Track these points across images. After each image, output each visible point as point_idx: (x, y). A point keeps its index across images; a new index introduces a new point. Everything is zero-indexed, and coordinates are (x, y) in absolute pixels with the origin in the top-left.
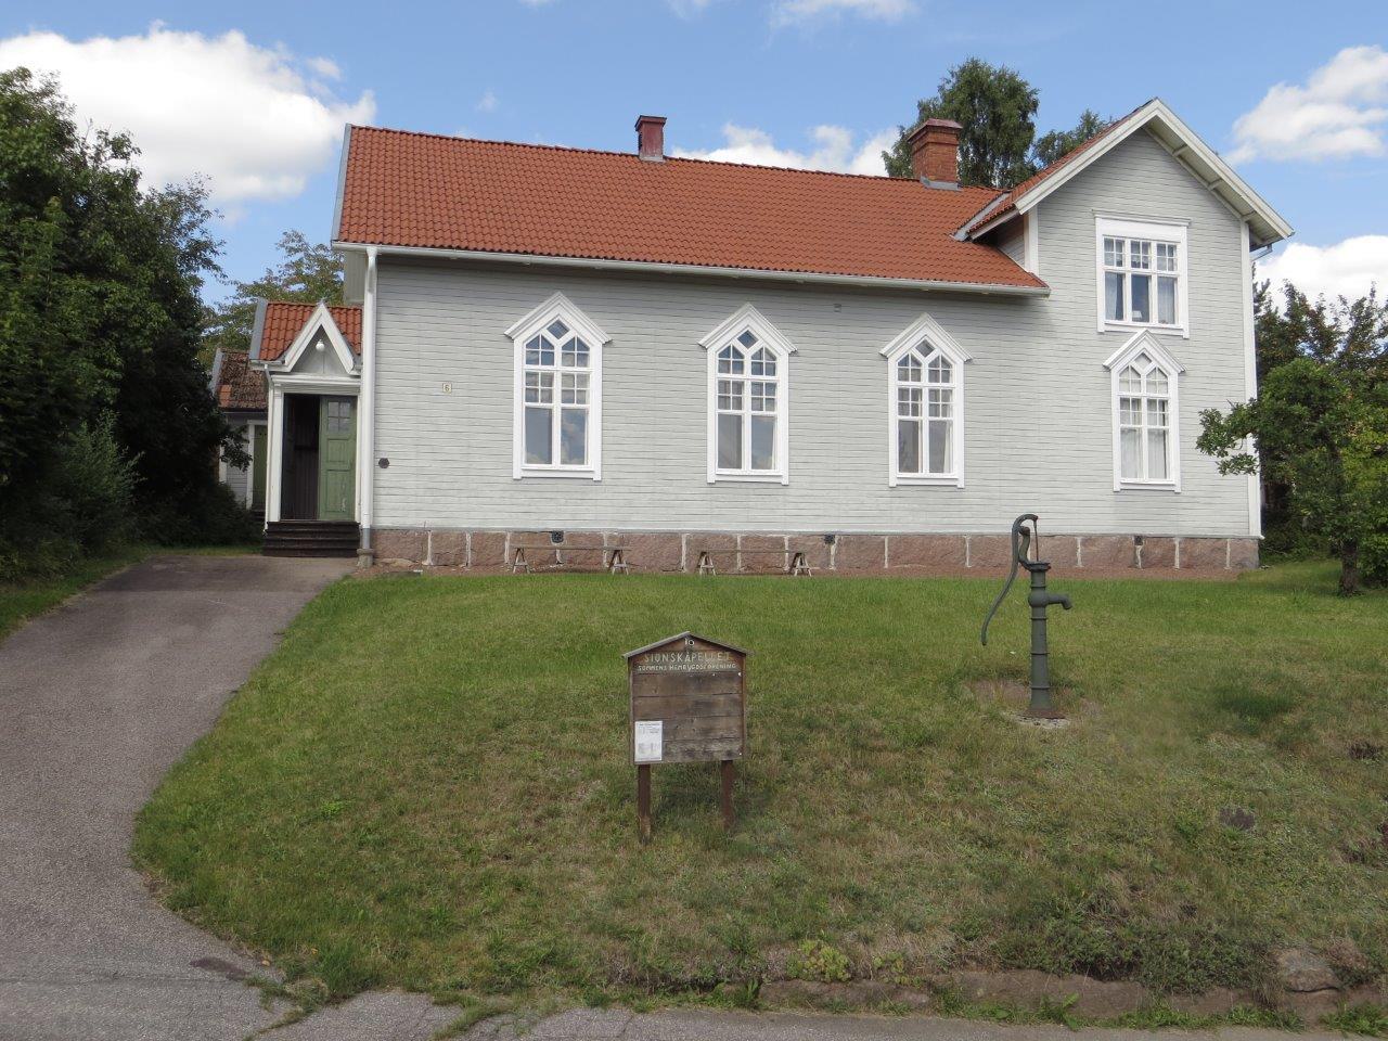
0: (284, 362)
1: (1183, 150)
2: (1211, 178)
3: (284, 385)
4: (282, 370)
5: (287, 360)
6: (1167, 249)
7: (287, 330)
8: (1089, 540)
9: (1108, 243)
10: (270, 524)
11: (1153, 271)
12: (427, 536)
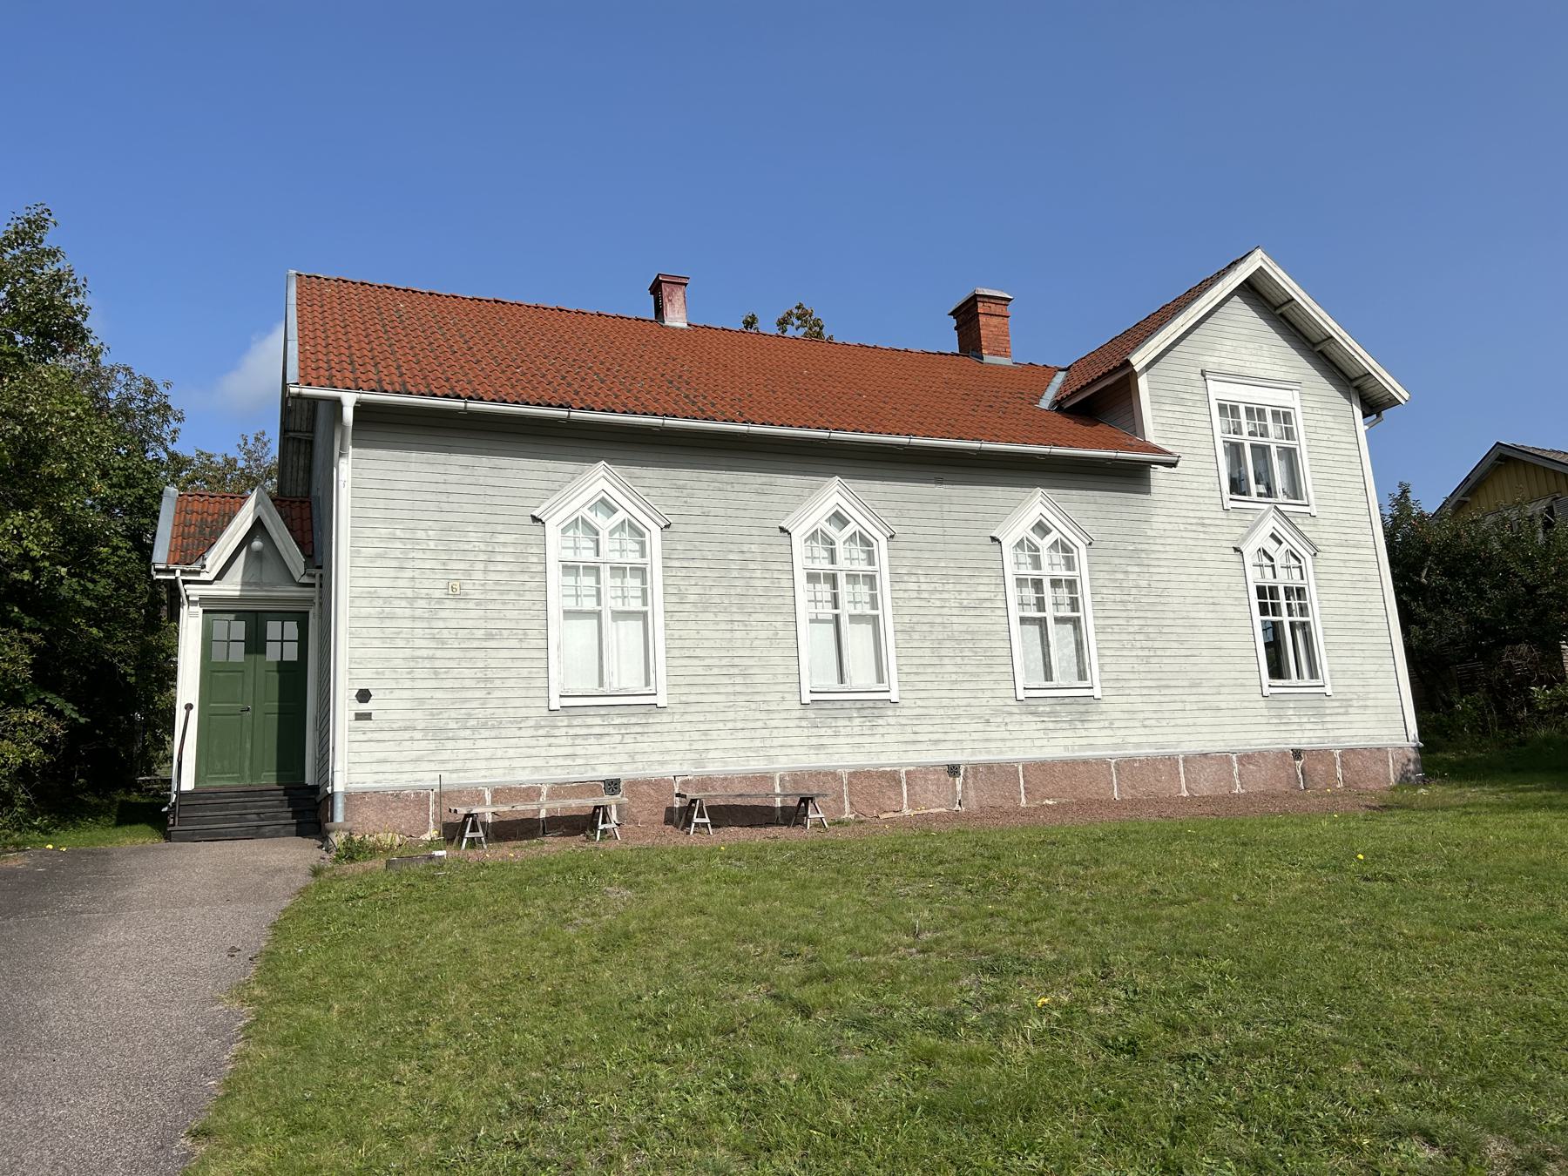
0: (204, 566)
1: (1290, 305)
2: (1316, 338)
3: (203, 600)
4: (203, 577)
5: (208, 563)
6: (1283, 416)
7: (302, 520)
8: (1246, 758)
9: (1222, 408)
10: (180, 794)
11: (1274, 440)
12: (428, 796)
